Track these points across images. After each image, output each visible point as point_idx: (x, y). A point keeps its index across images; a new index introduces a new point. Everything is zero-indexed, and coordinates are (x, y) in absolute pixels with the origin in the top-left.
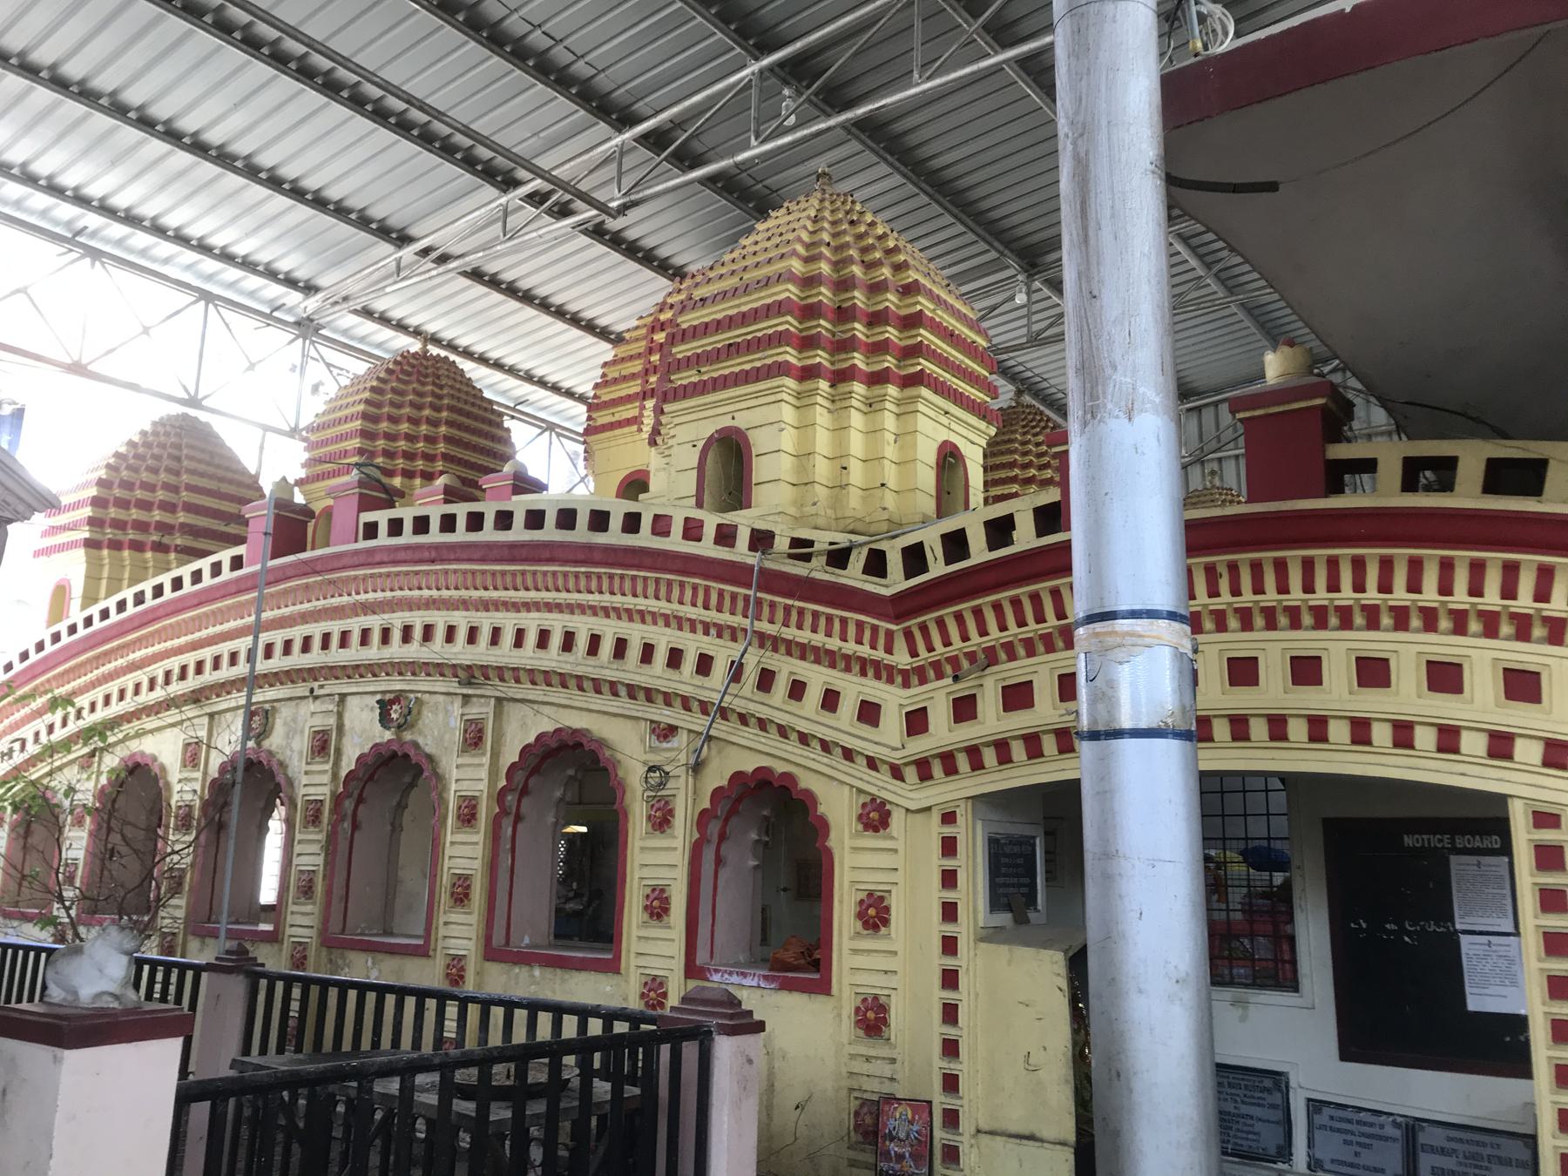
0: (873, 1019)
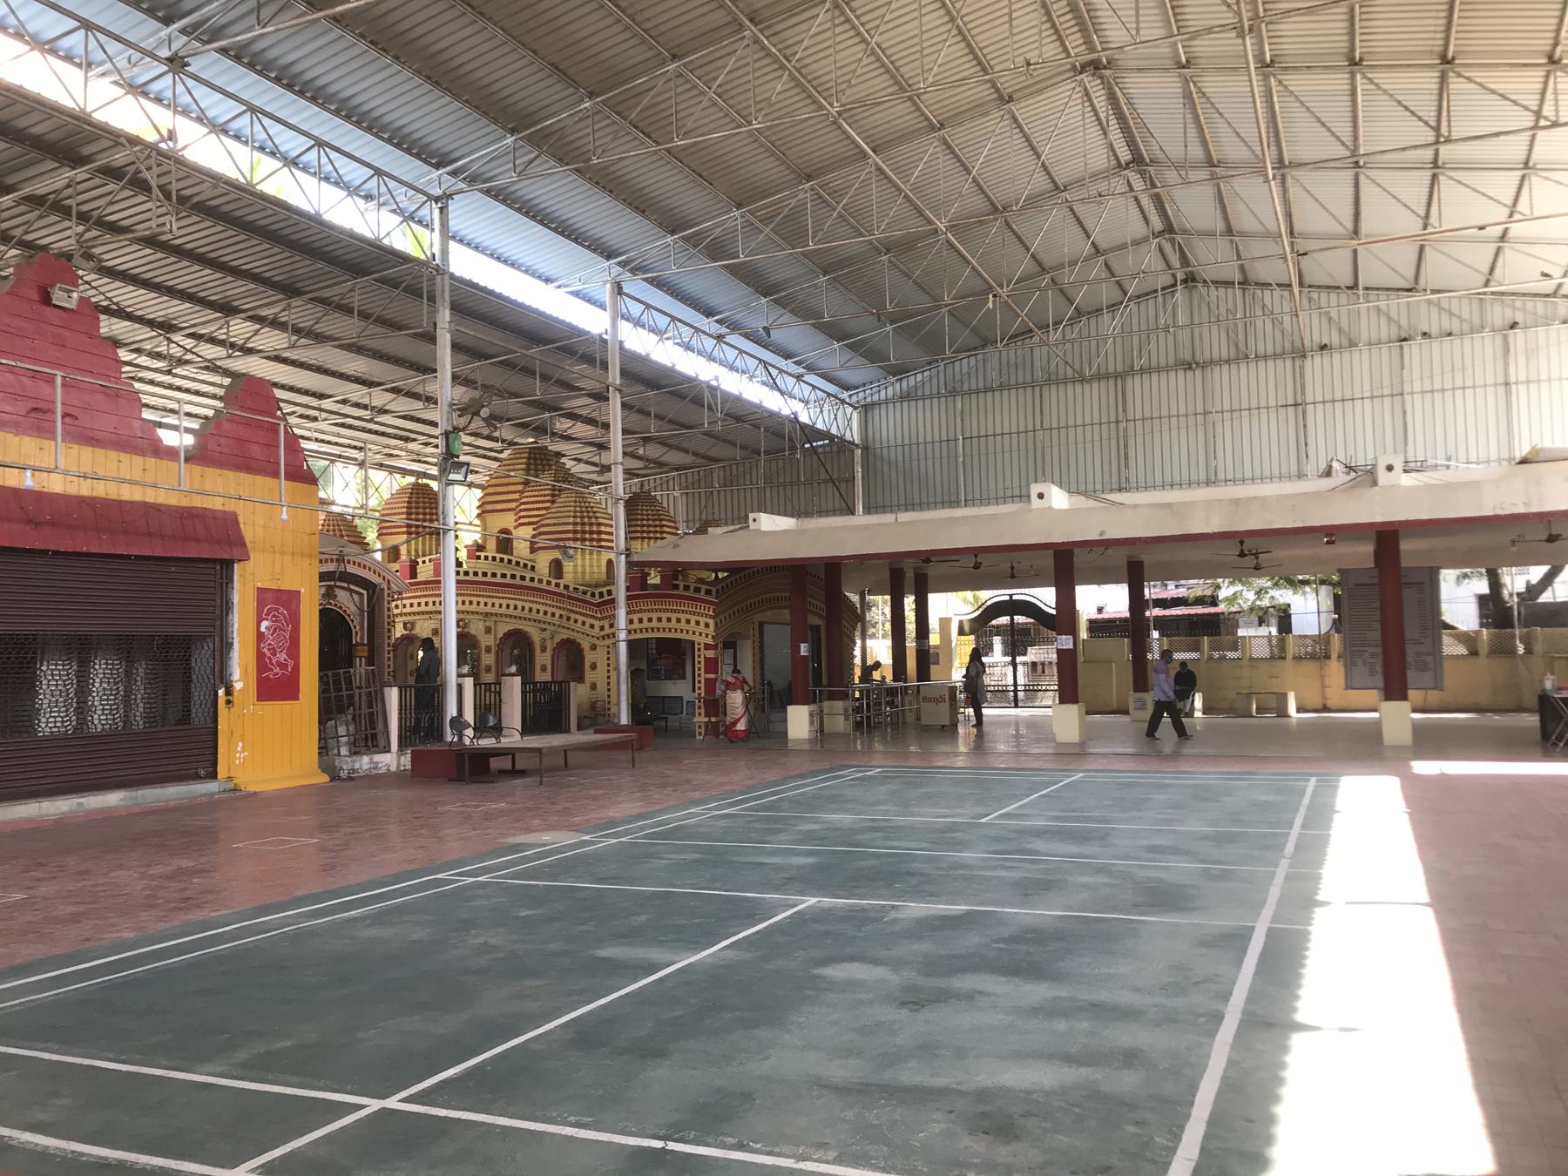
0: (594, 687)
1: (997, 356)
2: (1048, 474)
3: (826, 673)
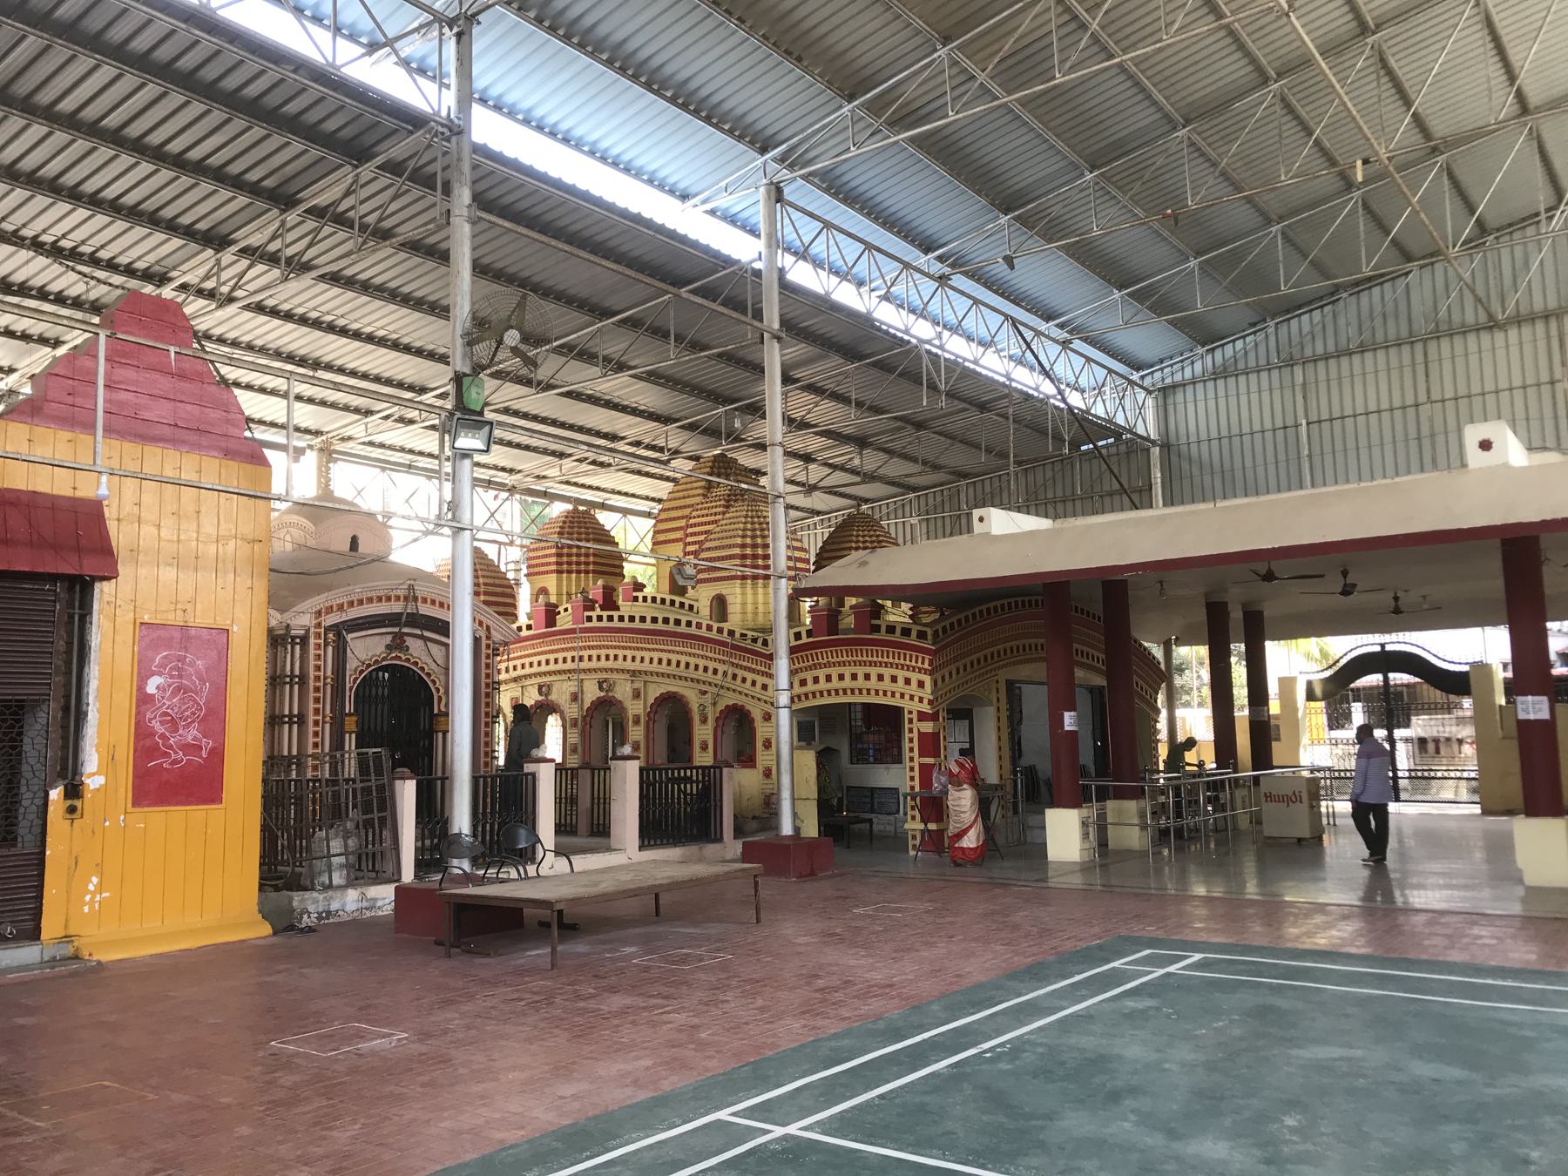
1: (1349, 310)
2: (1442, 460)
3: (1113, 758)
